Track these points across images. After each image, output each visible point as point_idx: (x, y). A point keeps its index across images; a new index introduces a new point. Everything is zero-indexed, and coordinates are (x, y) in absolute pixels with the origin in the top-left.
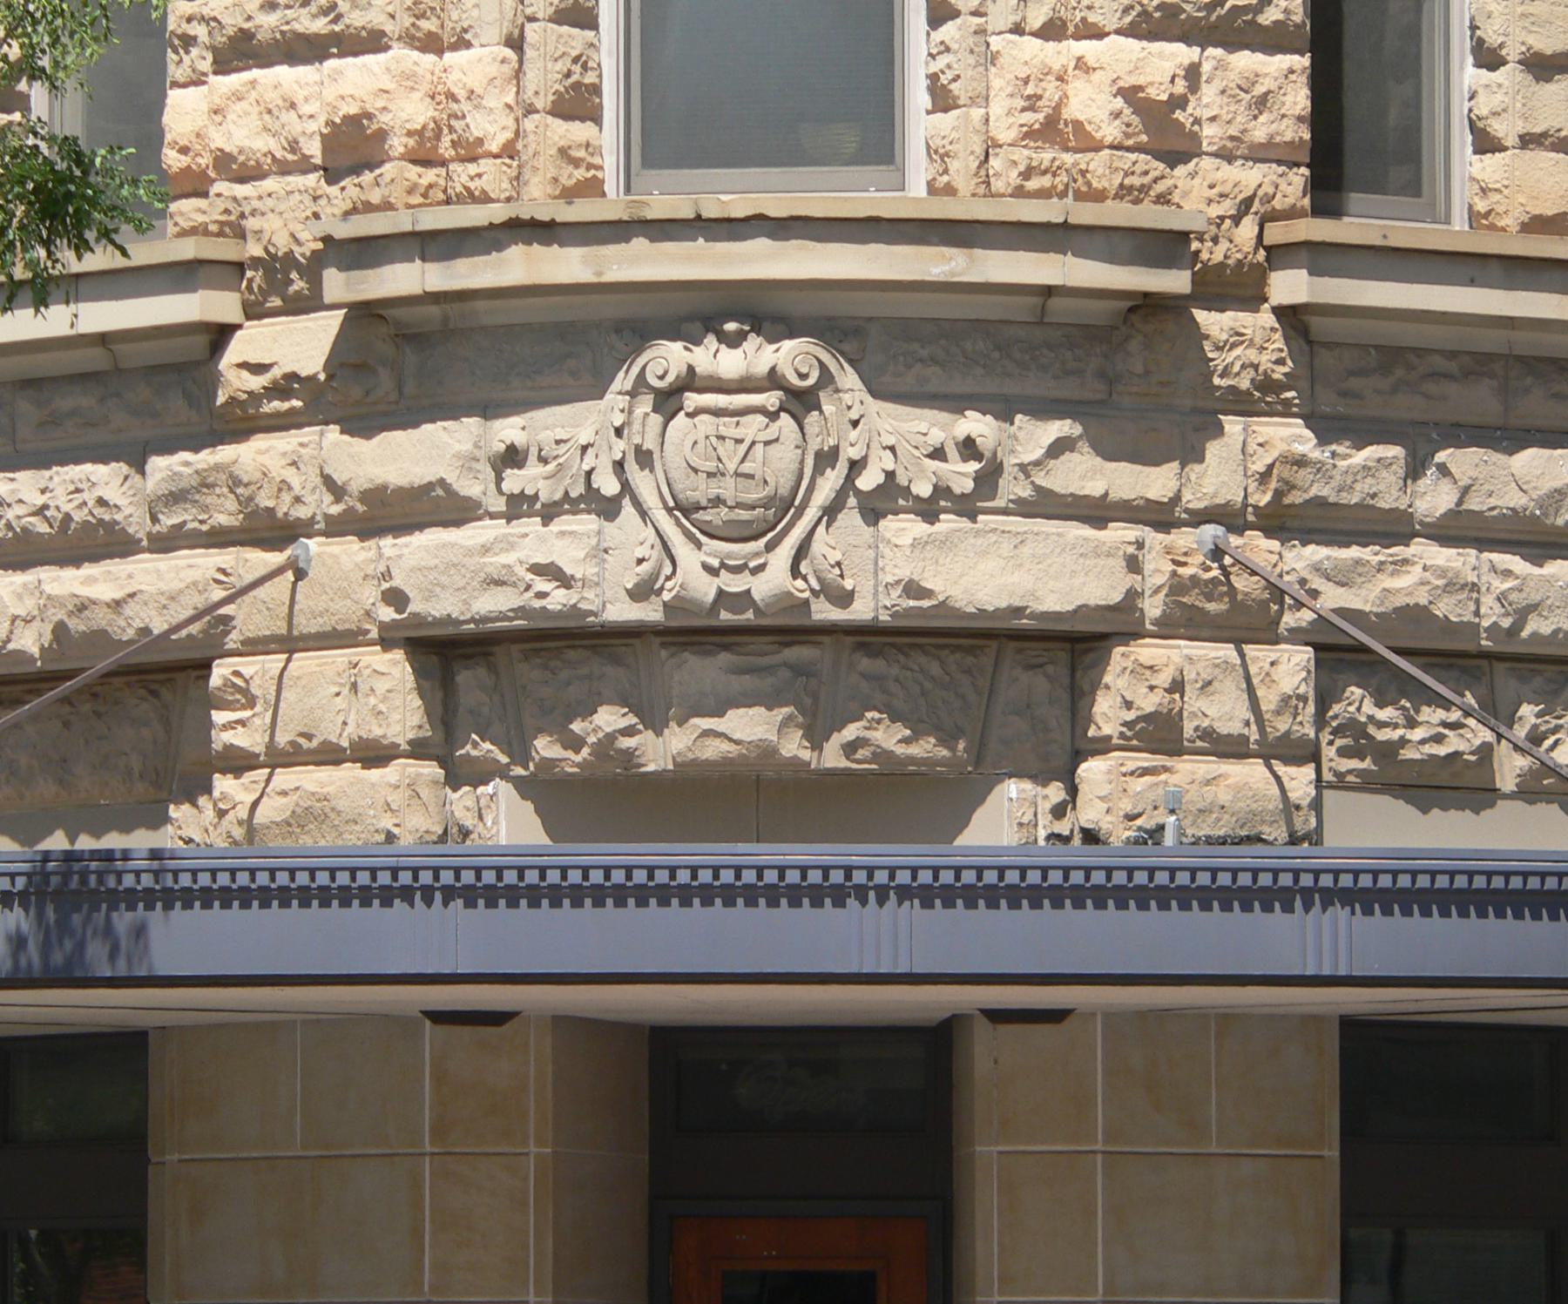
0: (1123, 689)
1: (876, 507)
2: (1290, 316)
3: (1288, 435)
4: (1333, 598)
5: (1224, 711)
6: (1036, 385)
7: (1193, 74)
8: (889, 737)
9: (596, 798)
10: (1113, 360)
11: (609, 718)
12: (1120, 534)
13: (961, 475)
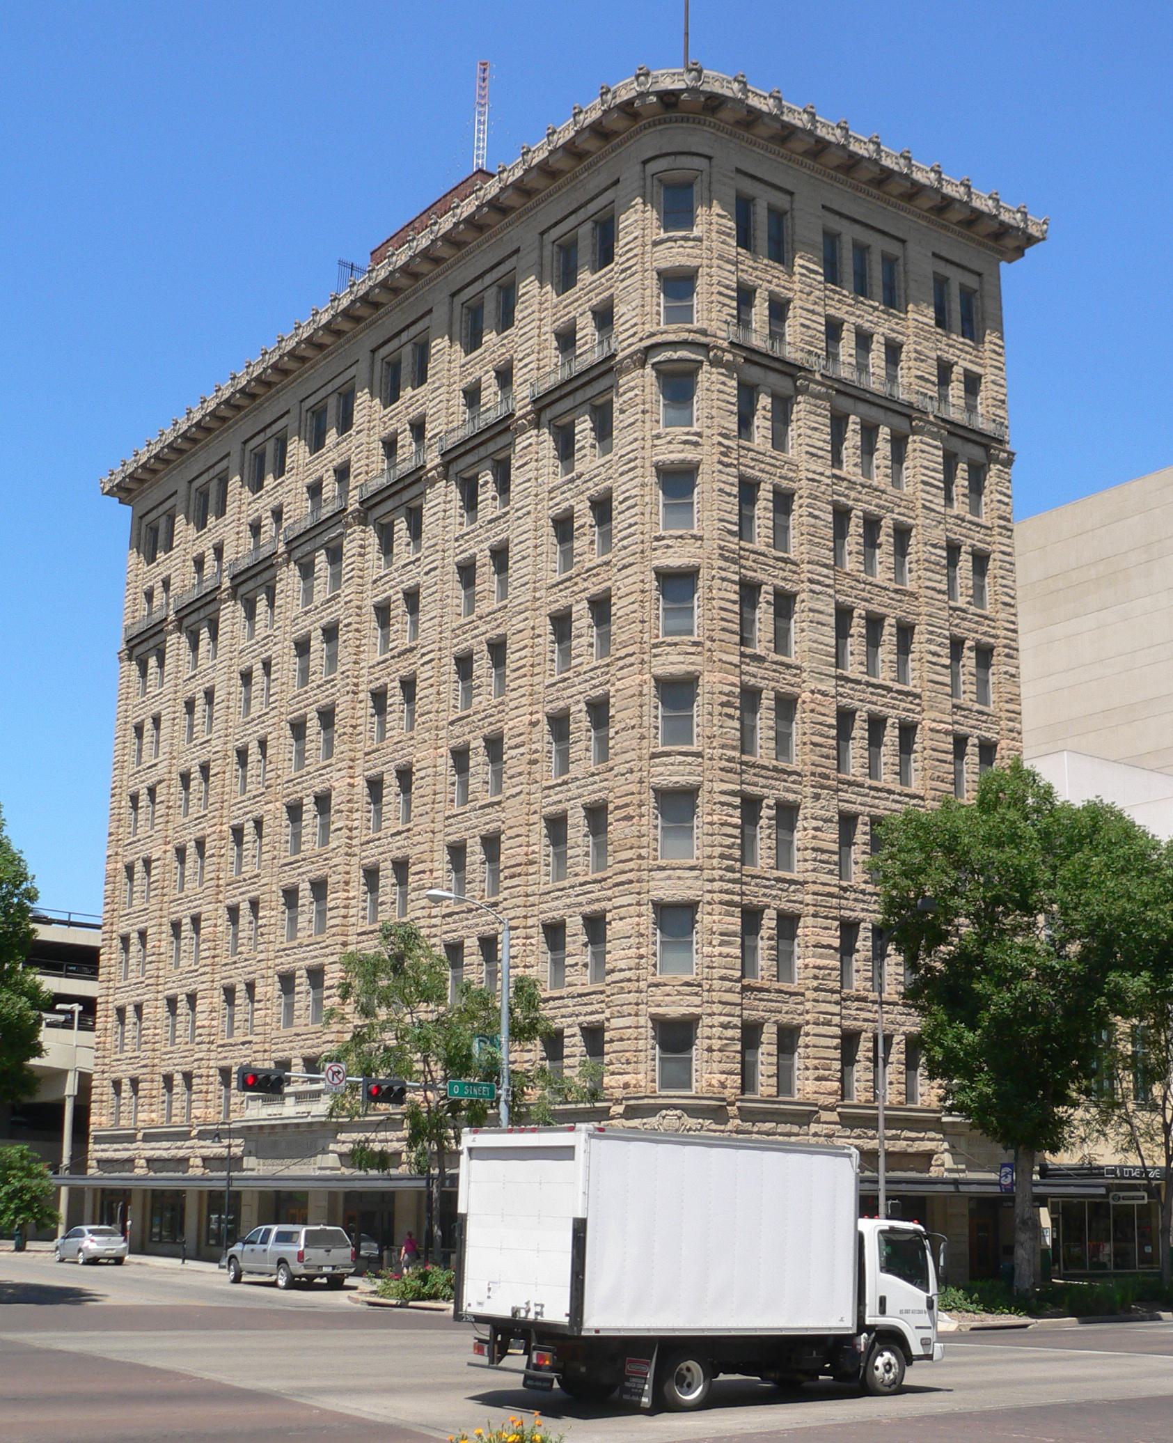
3: (739, 1121)
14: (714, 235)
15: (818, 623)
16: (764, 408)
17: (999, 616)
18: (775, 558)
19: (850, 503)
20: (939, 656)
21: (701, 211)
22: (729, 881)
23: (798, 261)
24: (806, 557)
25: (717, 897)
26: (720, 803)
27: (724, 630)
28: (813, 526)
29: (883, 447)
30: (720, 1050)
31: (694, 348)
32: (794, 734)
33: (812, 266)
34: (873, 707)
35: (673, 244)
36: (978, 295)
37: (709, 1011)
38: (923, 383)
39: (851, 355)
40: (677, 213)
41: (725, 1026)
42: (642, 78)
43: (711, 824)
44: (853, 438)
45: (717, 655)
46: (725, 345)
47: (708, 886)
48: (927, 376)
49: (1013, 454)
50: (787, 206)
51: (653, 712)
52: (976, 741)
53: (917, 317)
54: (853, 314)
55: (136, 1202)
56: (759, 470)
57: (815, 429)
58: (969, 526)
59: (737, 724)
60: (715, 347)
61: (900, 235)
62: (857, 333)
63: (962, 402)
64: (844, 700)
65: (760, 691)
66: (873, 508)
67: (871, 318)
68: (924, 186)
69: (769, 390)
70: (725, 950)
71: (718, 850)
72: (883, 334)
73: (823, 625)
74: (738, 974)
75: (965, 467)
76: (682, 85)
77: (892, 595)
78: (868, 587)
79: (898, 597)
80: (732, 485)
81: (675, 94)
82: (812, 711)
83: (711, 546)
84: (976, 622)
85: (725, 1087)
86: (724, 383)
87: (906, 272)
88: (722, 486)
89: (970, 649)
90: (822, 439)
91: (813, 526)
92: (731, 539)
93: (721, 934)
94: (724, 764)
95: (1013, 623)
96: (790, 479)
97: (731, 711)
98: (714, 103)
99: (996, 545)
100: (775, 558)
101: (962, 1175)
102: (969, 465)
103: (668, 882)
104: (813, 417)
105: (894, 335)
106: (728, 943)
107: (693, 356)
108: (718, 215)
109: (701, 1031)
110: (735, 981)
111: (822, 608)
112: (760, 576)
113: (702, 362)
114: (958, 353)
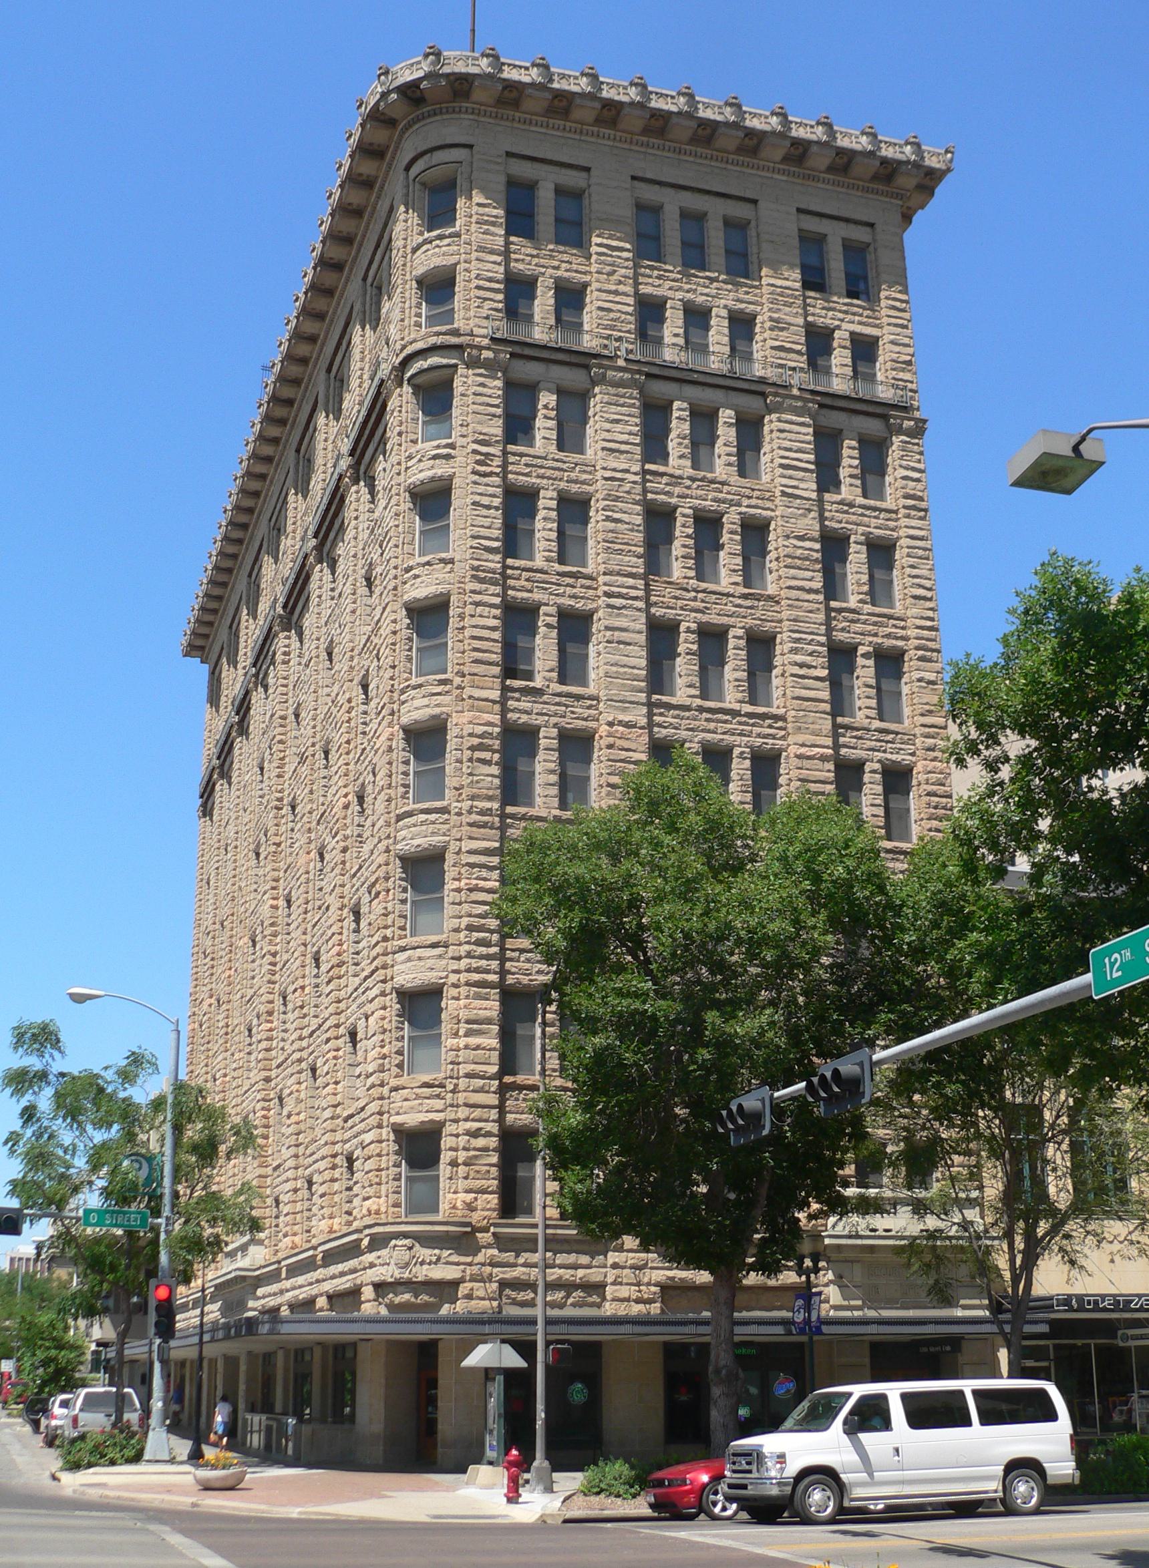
0: (463, 1290)
1: (422, 1263)
2: (494, 1234)
3: (495, 1252)
4: (501, 1276)
5: (481, 1293)
6: (447, 1245)
7: (476, 1199)
8: (426, 1298)
9: (391, 1307)
10: (462, 1240)
11: (391, 1295)
12: (462, 1267)
13: (434, 1259)
14: (474, 227)
15: (619, 642)
16: (546, 407)
17: (909, 613)
18: (558, 574)
19: (674, 500)
20: (810, 667)
21: (461, 203)
22: (481, 957)
23: (595, 240)
24: (602, 568)
25: (463, 977)
26: (468, 864)
27: (476, 661)
28: (612, 531)
29: (726, 433)
30: (465, 1164)
31: (445, 352)
32: (592, 777)
33: (614, 243)
34: (709, 736)
35: (428, 246)
36: (871, 248)
37: (453, 1116)
38: (783, 354)
39: (676, 335)
40: (439, 214)
41: (475, 1134)
42: (383, 78)
43: (459, 890)
44: (679, 426)
45: (468, 691)
46: (486, 342)
47: (455, 965)
48: (788, 345)
49: (925, 421)
50: (582, 184)
51: (402, 768)
52: (877, 766)
53: (772, 281)
54: (680, 289)
55: (188, 1365)
56: (538, 477)
57: (617, 421)
58: (860, 511)
59: (495, 770)
60: (469, 346)
61: (748, 195)
62: (685, 311)
63: (849, 371)
64: (664, 732)
65: (537, 729)
66: (708, 503)
67: (706, 291)
68: (764, 133)
69: (554, 387)
70: (473, 1041)
71: (465, 921)
72: (725, 307)
73: (629, 644)
74: (494, 1069)
75: (854, 443)
76: (421, 74)
77: (739, 601)
78: (700, 595)
79: (748, 603)
80: (494, 496)
81: (415, 84)
82: (610, 747)
83: (463, 568)
84: (875, 624)
85: (473, 1210)
86: (482, 385)
87: (758, 235)
88: (477, 498)
89: (866, 656)
90: (629, 429)
91: (612, 531)
92: (491, 557)
93: (468, 1022)
94: (475, 817)
95: (932, 619)
96: (583, 483)
97: (486, 755)
98: (461, 85)
99: (904, 530)
100: (558, 574)
101: (856, 1313)
102: (859, 442)
103: (409, 964)
104: (613, 408)
105: (743, 306)
106: (479, 1033)
107: (445, 361)
108: (479, 205)
109: (446, 1142)
110: (489, 1078)
111: (625, 625)
112: (537, 596)
113: (456, 366)
114: (841, 315)
